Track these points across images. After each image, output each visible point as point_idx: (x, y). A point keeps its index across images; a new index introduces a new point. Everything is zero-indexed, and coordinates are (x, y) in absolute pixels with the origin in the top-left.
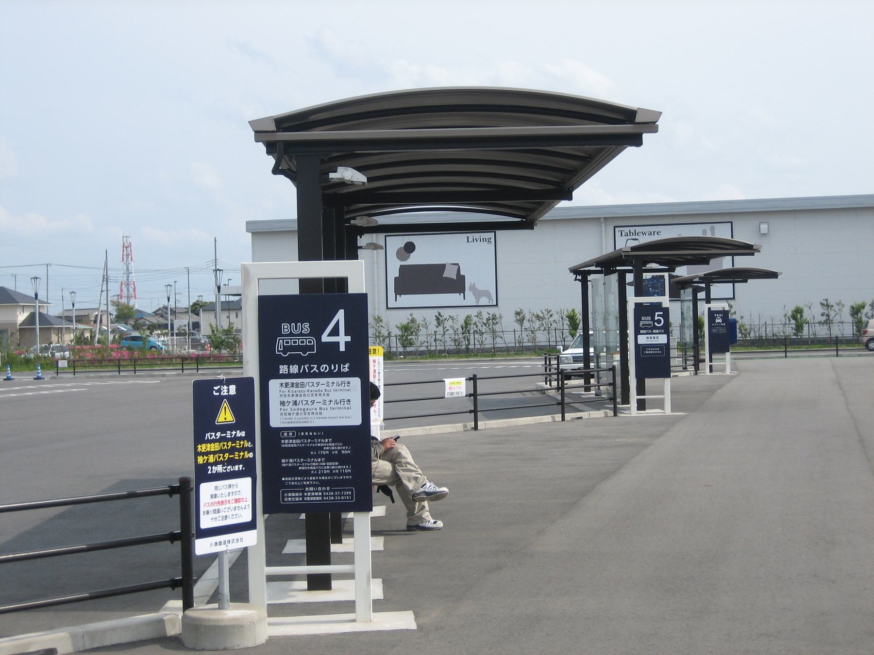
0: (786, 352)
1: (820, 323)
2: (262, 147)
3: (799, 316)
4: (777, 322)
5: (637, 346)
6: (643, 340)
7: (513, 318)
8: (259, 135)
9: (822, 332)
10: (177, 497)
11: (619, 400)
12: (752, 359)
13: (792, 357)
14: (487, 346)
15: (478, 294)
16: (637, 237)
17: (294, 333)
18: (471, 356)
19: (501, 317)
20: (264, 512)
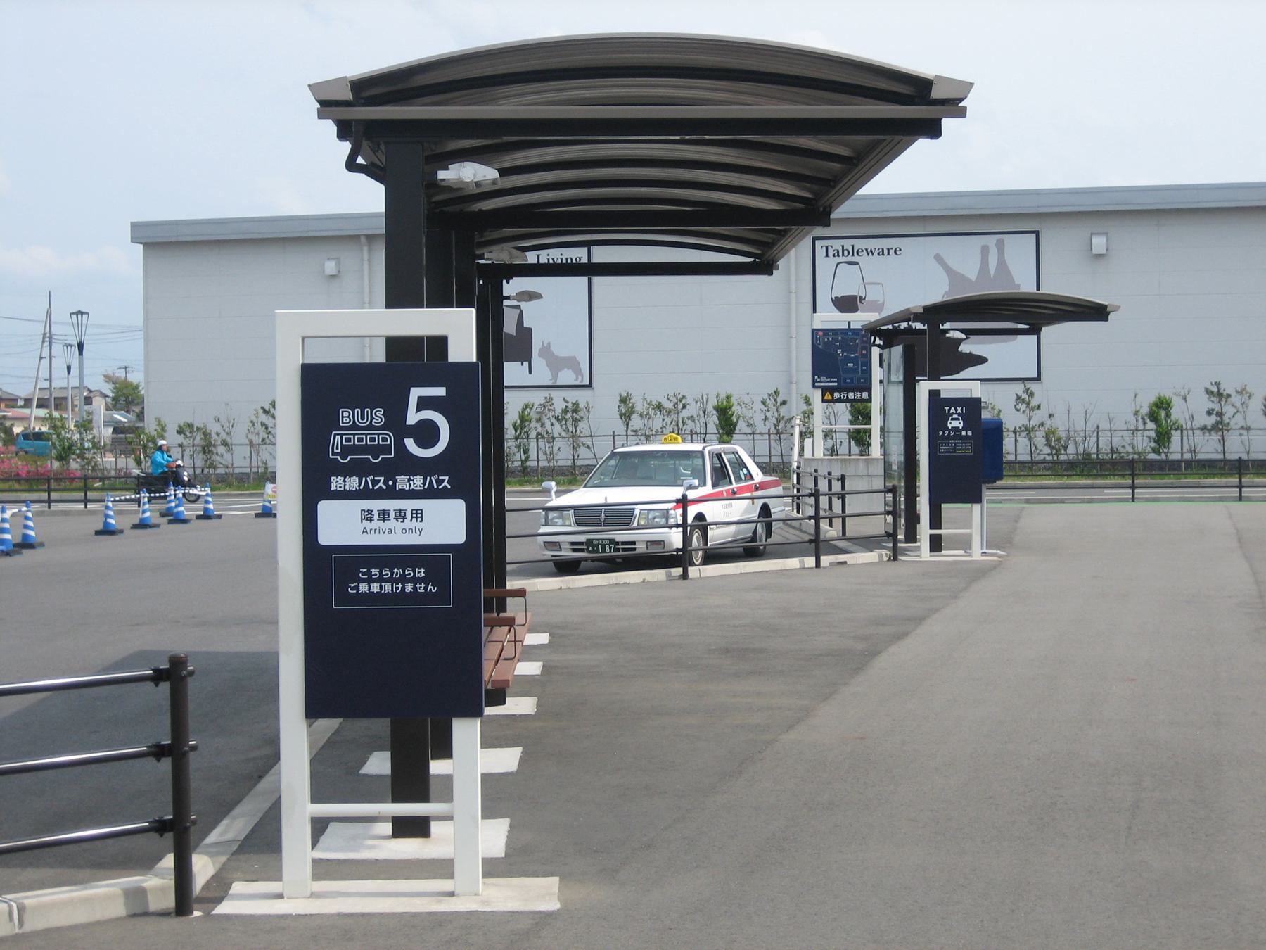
0: (1133, 487)
1: (1204, 428)
2: (330, 127)
3: (1163, 414)
4: (1119, 424)
5: (317, 558)
6: (342, 524)
7: (613, 407)
8: (327, 106)
9: (1208, 448)
10: (165, 687)
11: (901, 537)
12: (1062, 501)
13: (1147, 500)
14: (561, 463)
15: (556, 363)
16: (856, 259)
17: (359, 424)
18: (529, 482)
19: (588, 408)
20: (314, 709)
